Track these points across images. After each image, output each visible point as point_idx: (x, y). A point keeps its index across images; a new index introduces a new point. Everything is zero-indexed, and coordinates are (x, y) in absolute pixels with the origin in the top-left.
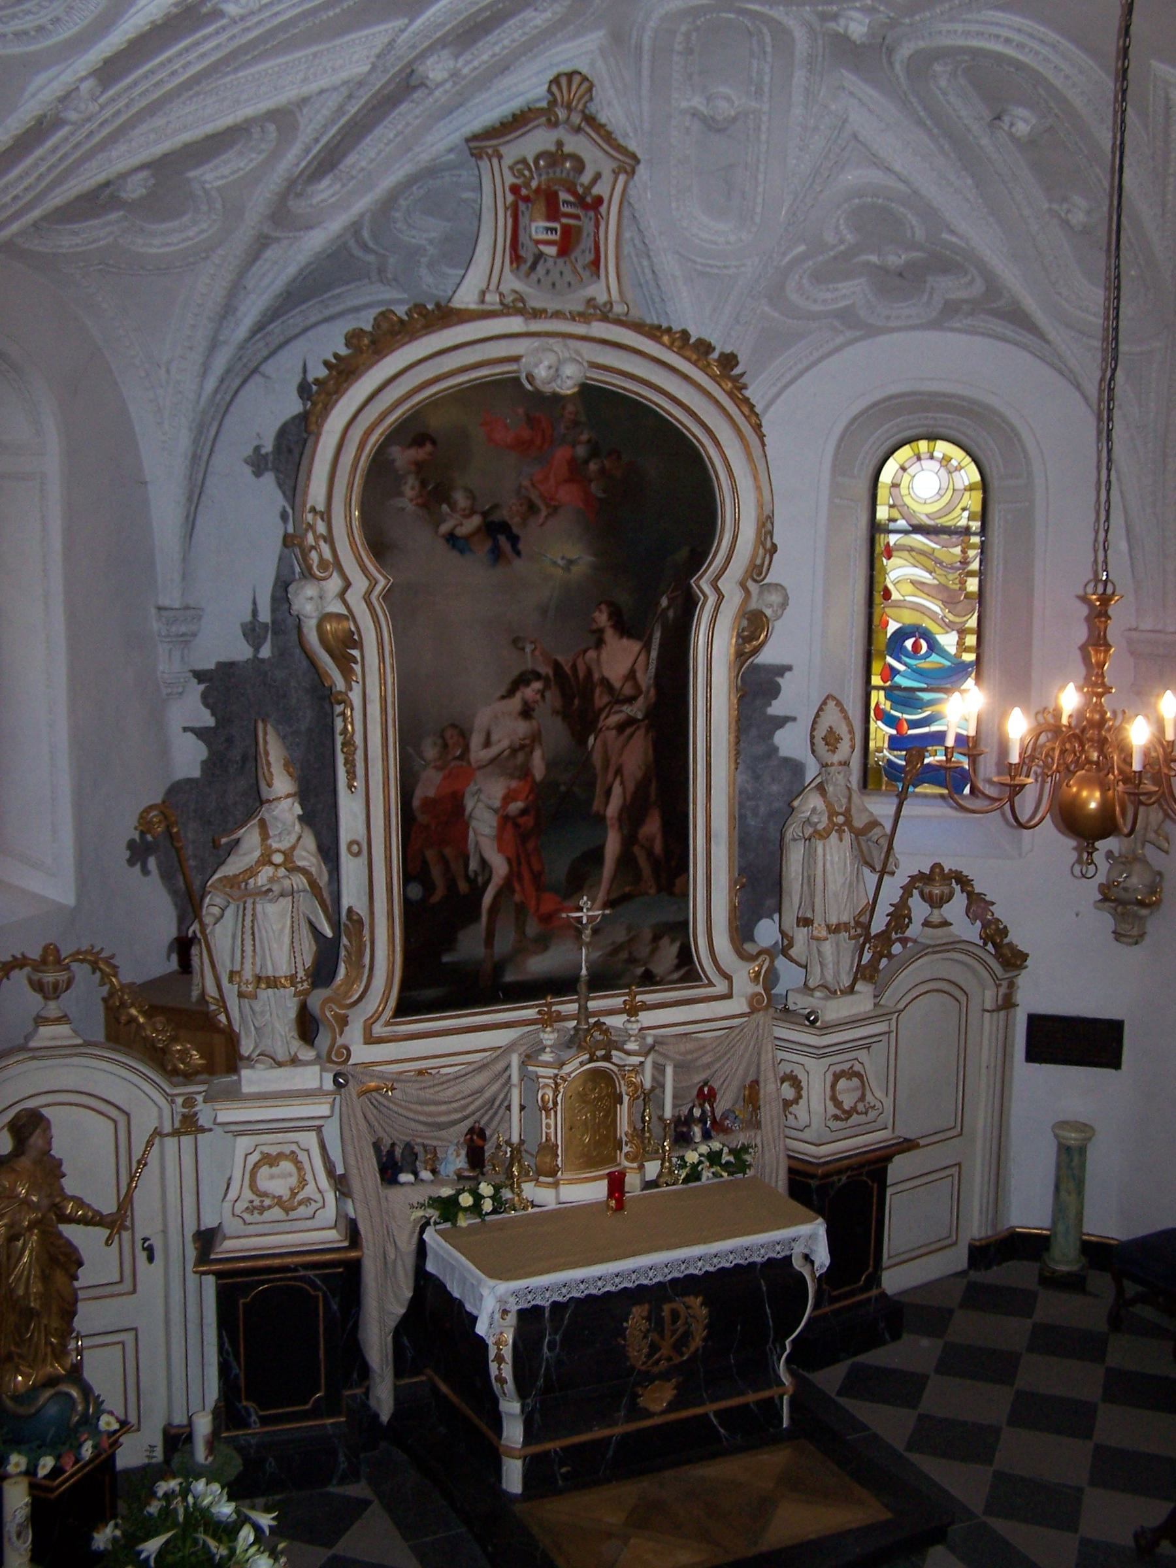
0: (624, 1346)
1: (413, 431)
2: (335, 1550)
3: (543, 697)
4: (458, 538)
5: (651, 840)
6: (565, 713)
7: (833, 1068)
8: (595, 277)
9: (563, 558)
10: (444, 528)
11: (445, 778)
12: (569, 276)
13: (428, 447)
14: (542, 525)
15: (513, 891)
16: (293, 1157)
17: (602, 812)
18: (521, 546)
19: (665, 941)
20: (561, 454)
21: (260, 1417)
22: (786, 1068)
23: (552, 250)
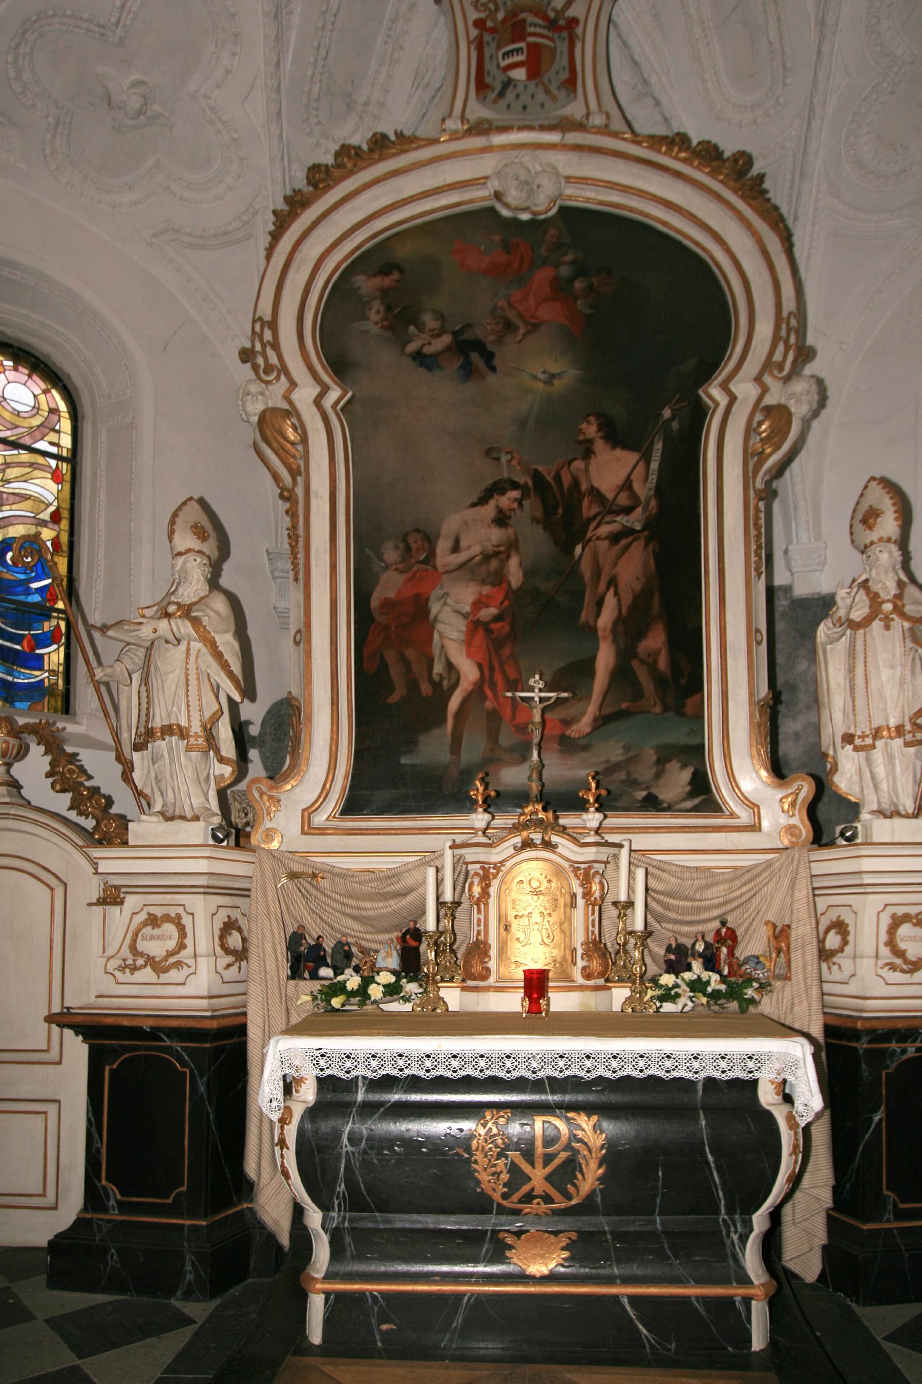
0: (468, 1161)
1: (377, 259)
2: (70, 1359)
3: (520, 505)
4: (425, 356)
5: (655, 655)
6: (547, 522)
7: (891, 910)
8: (572, 95)
9: (544, 372)
10: (411, 347)
11: (407, 581)
12: (541, 97)
13: (396, 275)
14: (520, 342)
15: (485, 698)
16: (177, 921)
17: (591, 622)
18: (496, 362)
19: (673, 766)
20: (542, 276)
21: (118, 1202)
22: (833, 915)
23: (520, 74)
